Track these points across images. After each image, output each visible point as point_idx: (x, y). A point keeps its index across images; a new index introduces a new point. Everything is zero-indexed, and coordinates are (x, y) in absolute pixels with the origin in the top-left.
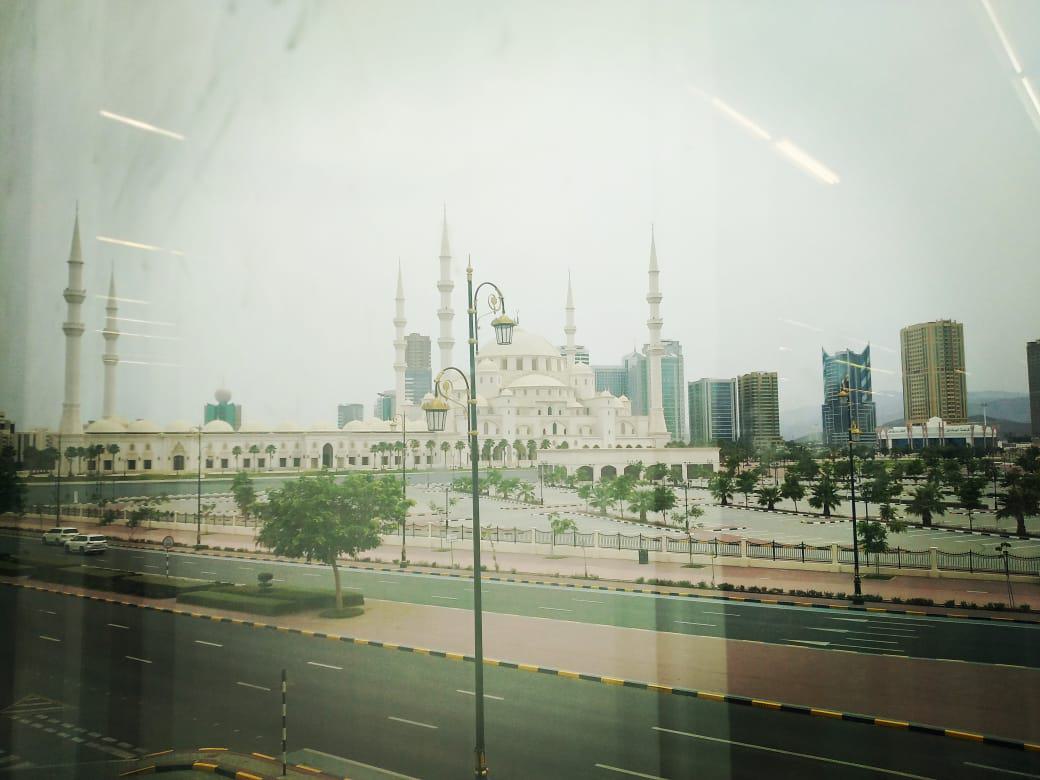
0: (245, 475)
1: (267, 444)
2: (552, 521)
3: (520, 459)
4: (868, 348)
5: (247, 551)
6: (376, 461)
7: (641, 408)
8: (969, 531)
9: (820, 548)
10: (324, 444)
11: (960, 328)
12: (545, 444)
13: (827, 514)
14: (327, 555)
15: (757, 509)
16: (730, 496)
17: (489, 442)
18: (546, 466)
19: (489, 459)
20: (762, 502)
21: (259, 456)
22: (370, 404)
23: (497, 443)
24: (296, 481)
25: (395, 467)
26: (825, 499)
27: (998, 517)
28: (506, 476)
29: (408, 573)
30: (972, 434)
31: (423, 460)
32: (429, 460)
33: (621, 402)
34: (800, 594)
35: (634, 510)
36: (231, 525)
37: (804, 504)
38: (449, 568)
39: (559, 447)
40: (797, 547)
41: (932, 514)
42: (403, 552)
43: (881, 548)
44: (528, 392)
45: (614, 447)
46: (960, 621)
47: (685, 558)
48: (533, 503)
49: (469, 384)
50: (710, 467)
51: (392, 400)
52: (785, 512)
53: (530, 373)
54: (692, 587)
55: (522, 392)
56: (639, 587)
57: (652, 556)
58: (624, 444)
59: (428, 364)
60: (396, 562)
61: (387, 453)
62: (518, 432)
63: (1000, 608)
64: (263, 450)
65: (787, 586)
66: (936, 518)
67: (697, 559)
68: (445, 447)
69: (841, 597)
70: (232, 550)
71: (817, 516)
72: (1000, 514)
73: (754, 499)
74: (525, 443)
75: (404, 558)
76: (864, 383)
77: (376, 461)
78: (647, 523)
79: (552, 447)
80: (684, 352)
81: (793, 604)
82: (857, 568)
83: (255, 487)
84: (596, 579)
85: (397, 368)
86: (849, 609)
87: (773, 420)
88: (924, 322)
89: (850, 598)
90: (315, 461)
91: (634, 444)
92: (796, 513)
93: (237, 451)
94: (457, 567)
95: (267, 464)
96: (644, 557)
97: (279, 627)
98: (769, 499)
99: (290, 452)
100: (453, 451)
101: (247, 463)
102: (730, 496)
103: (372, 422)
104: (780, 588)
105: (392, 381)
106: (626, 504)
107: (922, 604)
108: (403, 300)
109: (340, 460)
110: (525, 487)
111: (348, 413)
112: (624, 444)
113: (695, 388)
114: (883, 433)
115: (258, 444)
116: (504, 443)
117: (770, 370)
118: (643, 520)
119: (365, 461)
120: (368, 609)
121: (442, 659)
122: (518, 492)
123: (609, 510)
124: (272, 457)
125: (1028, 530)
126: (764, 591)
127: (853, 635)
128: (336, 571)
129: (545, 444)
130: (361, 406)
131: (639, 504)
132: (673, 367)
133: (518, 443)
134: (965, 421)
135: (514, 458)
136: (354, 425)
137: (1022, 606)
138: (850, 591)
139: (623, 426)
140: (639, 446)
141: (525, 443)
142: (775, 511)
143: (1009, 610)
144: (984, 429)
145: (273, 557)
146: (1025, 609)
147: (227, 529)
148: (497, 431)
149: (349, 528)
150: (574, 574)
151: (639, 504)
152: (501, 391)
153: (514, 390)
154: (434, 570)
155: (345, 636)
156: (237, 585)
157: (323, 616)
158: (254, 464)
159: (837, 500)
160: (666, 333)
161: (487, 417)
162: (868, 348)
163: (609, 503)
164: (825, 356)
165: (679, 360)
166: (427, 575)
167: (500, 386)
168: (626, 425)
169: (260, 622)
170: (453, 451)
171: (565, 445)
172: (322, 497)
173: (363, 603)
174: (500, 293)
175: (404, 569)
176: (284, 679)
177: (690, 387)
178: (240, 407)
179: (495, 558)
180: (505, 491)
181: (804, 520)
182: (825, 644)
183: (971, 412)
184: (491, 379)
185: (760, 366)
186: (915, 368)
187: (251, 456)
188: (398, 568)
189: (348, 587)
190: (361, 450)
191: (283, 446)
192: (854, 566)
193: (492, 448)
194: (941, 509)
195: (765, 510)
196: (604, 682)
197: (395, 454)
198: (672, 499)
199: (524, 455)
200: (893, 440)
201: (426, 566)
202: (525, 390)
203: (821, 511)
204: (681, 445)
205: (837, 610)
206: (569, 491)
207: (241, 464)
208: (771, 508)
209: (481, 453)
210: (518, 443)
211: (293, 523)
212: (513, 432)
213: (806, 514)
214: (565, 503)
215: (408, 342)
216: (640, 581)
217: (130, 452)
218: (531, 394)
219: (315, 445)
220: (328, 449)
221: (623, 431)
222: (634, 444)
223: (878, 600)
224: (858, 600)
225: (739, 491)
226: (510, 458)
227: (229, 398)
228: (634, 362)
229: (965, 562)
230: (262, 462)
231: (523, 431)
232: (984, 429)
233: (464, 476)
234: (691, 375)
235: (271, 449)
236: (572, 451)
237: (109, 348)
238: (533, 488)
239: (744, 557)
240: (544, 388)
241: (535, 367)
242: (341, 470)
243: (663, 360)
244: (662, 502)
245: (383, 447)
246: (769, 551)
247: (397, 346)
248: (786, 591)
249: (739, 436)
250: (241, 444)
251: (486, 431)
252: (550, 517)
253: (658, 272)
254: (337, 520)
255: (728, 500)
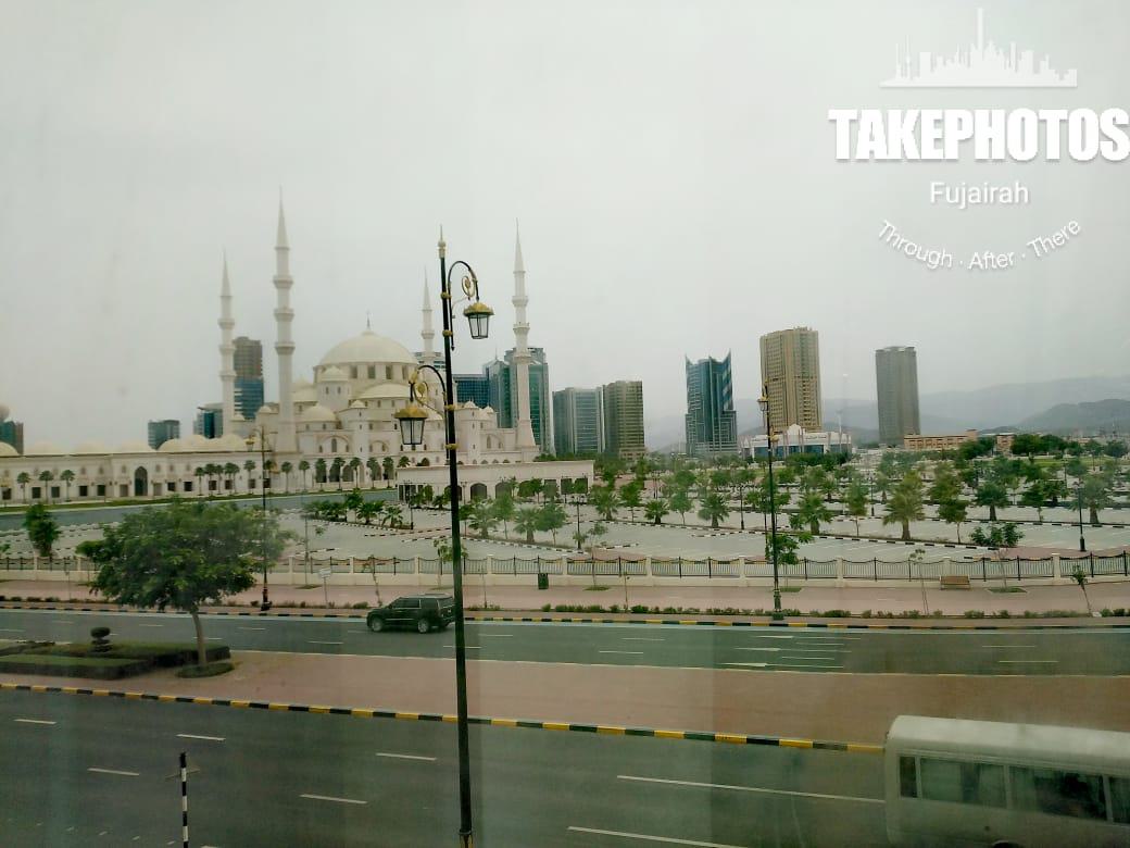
0: (40, 506)
1: (62, 470)
2: (439, 546)
3: (374, 479)
4: (729, 355)
5: (58, 601)
6: (201, 486)
7: (507, 419)
8: (856, 539)
9: (697, 562)
10: (136, 467)
11: (815, 335)
12: (404, 461)
13: (715, 526)
14: (188, 602)
15: (643, 524)
16: (615, 511)
17: (339, 461)
18: (407, 487)
19: (338, 480)
20: (649, 516)
21: (52, 484)
22: (188, 419)
23: (348, 462)
24: (164, 510)
25: (226, 493)
26: (715, 510)
27: (885, 523)
28: (367, 499)
29: (273, 616)
30: (829, 441)
31: (260, 483)
32: (267, 484)
33: (487, 414)
34: (717, 612)
35: (521, 530)
36: (32, 569)
37: (692, 517)
38: (322, 607)
39: (419, 465)
40: (673, 562)
41: (820, 522)
42: (265, 592)
43: (791, 559)
44: (382, 404)
45: (479, 463)
46: (881, 631)
47: (588, 581)
48: (400, 527)
49: (445, 382)
50: (585, 480)
51: (217, 416)
52: (673, 526)
53: (382, 383)
54: (604, 611)
55: (390, 403)
56: (547, 615)
57: (552, 580)
58: (490, 459)
59: (259, 371)
60: (254, 604)
61: (215, 477)
62: (371, 448)
63: (915, 616)
64: (57, 477)
65: (704, 605)
66: (823, 526)
67: (602, 581)
68: (287, 467)
69: (759, 613)
70: (38, 600)
71: (706, 528)
72: (886, 520)
73: (641, 514)
74: (380, 462)
75: (265, 599)
76: (725, 391)
77: (201, 486)
78: (534, 544)
79: (412, 465)
80: (548, 360)
81: (713, 624)
82: (776, 580)
83: (57, 522)
84: (497, 609)
85: (224, 377)
86: (771, 625)
87: (639, 436)
88: (781, 330)
89: (768, 614)
90: (125, 488)
91: (500, 459)
92: (684, 526)
93: (23, 478)
94: (332, 606)
95: (64, 493)
96: (543, 583)
97: (162, 696)
98: (655, 515)
99: (92, 477)
100: (297, 472)
101: (36, 492)
102: (615, 511)
103: (189, 438)
104: (696, 607)
105: (217, 391)
106: (511, 525)
107: (839, 616)
108: (223, 297)
109: (157, 486)
110: (390, 510)
111: (163, 432)
112: (490, 459)
113: (560, 399)
114: (746, 441)
115: (50, 470)
116: (356, 462)
117: (635, 379)
118: (530, 541)
119: (188, 486)
120: (238, 664)
121: (28, 692)
122: (384, 516)
123: (490, 531)
124: (69, 485)
125: (912, 535)
126: (680, 612)
127: (785, 653)
128: (196, 619)
129: (404, 461)
130: (176, 423)
131: (525, 523)
132: (539, 374)
133: (372, 463)
134: (820, 429)
135: (367, 479)
136: (169, 446)
137: (935, 613)
138: (770, 607)
139: (489, 439)
140: (506, 461)
141: (380, 462)
142: (663, 525)
143: (924, 617)
144: (840, 436)
145: (115, 607)
146: (938, 615)
147: (27, 574)
148: (347, 448)
149: (216, 568)
150: (471, 606)
151: (525, 523)
152: (350, 402)
153: (366, 402)
154: (305, 611)
155: (380, 710)
156: (58, 643)
157: (184, 675)
158: (46, 494)
159: (725, 511)
160: (533, 341)
161: (334, 433)
162: (729, 355)
163: (491, 525)
164: (688, 363)
165: (543, 369)
166: (296, 617)
167: (349, 397)
168: (492, 439)
169: (102, 688)
170: (297, 472)
171: (425, 462)
172: (180, 532)
173: (228, 656)
174: (473, 275)
175: (268, 612)
176: (183, 765)
177: (554, 397)
178: (21, 426)
179: (377, 593)
180: (366, 516)
181: (694, 533)
182: (763, 665)
183: (825, 418)
184: (327, 389)
185: (626, 375)
186: (772, 376)
187: (41, 484)
188: (257, 610)
189: (212, 639)
190: (182, 473)
191: (83, 471)
192: (773, 579)
193: (342, 468)
194: (828, 516)
195: (653, 525)
196: (547, 728)
197: (225, 477)
198: (563, 516)
199: (379, 474)
200: (756, 449)
201: (292, 606)
202: (379, 402)
203: (709, 523)
204: (551, 459)
205: (761, 626)
206: (439, 513)
207: (28, 494)
208: (658, 522)
209: (328, 474)
210: (372, 463)
211: (142, 565)
212: (366, 449)
213: (694, 528)
214: (429, 528)
215: (238, 347)
216: (547, 609)
217: (100, 476)
218: (386, 405)
219: (124, 469)
220: (142, 473)
221: (489, 446)
222: (500, 459)
223: (797, 614)
224: (778, 617)
225: (626, 505)
226: (362, 479)
227: (7, 415)
228: (495, 371)
229: (868, 570)
230: (56, 492)
231: (377, 448)
232: (840, 436)
233: (315, 500)
234: (556, 384)
235: (68, 475)
236: (432, 469)
237: (283, 298)
238: (400, 512)
239: (565, 576)
240: (386, 399)
241: (389, 376)
242: (158, 498)
243: (531, 369)
244: (552, 521)
245: (211, 469)
246: (390, 566)
247: (224, 351)
248: (703, 609)
249: (604, 447)
250: (29, 471)
251: (334, 449)
252: (436, 543)
253: (524, 272)
254: (201, 557)
255: (613, 515)
